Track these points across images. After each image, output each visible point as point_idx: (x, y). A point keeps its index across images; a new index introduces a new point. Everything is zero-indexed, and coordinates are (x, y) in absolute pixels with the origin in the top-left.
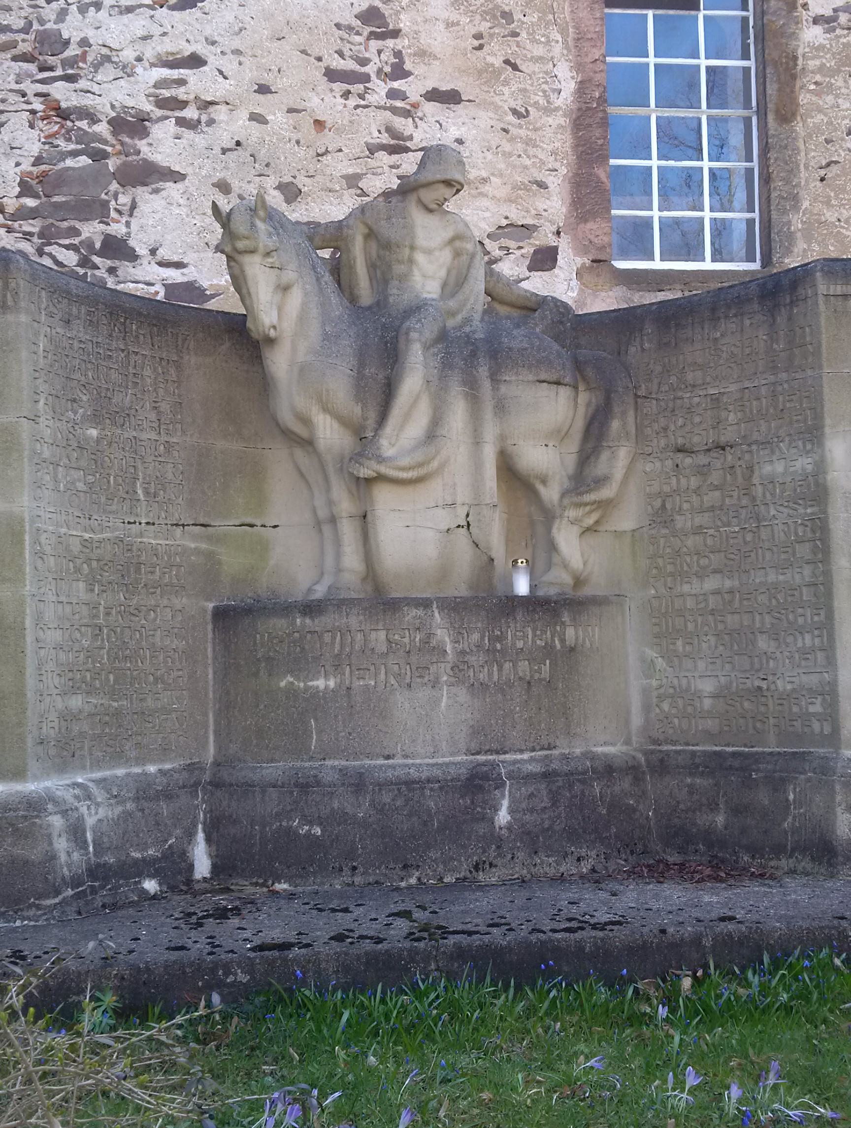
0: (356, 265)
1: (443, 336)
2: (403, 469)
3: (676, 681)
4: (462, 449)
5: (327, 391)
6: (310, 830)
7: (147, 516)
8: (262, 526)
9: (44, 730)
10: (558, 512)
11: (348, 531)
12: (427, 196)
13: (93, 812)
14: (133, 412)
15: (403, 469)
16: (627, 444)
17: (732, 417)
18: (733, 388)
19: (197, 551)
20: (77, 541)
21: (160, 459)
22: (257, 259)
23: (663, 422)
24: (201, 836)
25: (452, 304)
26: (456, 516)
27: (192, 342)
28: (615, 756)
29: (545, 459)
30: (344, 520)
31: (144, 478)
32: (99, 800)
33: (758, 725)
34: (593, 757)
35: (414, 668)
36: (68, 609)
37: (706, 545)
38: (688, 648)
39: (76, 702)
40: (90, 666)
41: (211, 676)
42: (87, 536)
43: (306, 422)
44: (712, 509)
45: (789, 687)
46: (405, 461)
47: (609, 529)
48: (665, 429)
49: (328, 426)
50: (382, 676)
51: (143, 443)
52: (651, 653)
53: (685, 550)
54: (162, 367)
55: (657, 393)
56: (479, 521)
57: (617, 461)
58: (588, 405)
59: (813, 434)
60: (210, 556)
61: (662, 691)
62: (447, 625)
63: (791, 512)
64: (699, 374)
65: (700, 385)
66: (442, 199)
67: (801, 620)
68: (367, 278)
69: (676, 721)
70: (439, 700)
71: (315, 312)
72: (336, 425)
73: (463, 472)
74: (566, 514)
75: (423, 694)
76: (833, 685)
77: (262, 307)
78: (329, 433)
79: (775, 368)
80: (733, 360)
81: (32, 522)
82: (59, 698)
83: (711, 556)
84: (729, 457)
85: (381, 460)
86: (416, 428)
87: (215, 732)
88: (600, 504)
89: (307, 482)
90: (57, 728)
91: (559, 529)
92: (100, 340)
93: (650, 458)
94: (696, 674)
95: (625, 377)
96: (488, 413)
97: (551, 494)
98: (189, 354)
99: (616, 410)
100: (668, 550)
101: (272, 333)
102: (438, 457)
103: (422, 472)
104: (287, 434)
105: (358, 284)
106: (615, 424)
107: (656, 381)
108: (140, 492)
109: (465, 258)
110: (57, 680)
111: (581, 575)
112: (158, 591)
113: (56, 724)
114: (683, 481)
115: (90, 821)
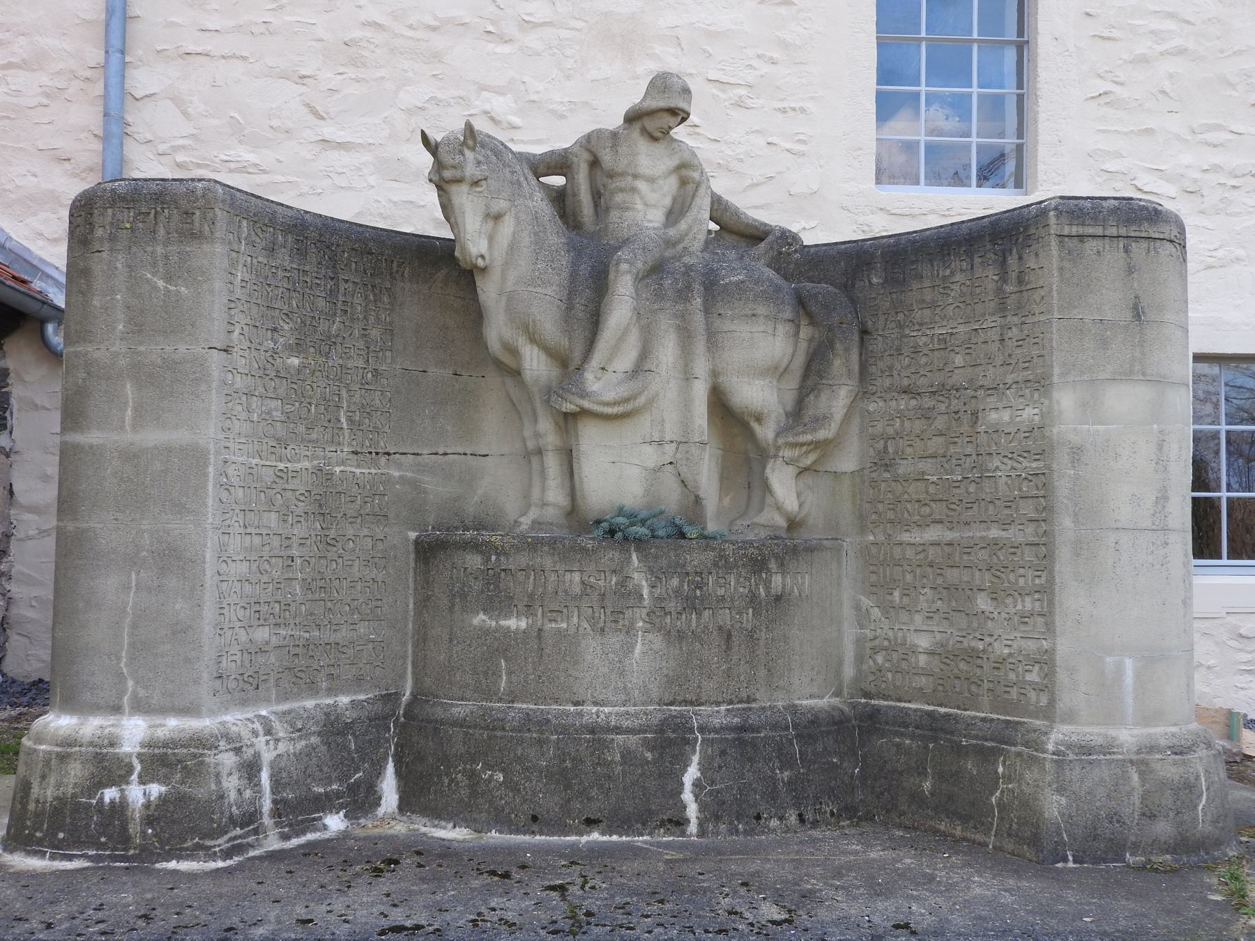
0: (577, 192)
2: (608, 404)
3: (891, 634)
4: (673, 383)
5: (534, 321)
6: (491, 776)
7: (350, 445)
9: (224, 664)
10: (772, 451)
11: (553, 464)
12: (651, 124)
13: (272, 747)
14: (340, 340)
15: (608, 404)
16: (850, 382)
17: (959, 360)
18: (961, 329)
20: (270, 471)
22: (464, 188)
24: (390, 768)
25: (672, 232)
26: (664, 453)
28: (821, 710)
29: (758, 394)
30: (550, 453)
32: (281, 734)
33: (973, 688)
34: (793, 709)
35: (608, 611)
36: (257, 540)
37: (927, 492)
38: (905, 600)
39: (262, 634)
40: (279, 598)
41: (411, 606)
42: (281, 466)
43: (514, 352)
45: (1006, 651)
46: (610, 396)
48: (891, 368)
49: (535, 356)
50: (575, 620)
52: (866, 602)
53: (906, 496)
54: (375, 295)
57: (837, 400)
58: (811, 340)
59: (1041, 384)
60: (415, 485)
61: (877, 642)
62: (644, 569)
63: (1015, 464)
67: (1021, 581)
68: (592, 205)
69: (890, 675)
70: (633, 647)
72: (543, 357)
73: (677, 406)
75: (615, 640)
76: (1051, 652)
77: (468, 237)
78: (535, 364)
79: (1005, 309)
81: (218, 452)
82: (242, 632)
85: (584, 395)
86: (625, 361)
87: (413, 663)
88: (816, 445)
89: (518, 412)
90: (239, 663)
92: (307, 268)
93: (874, 398)
94: (912, 628)
96: (700, 346)
97: (766, 432)
101: (480, 263)
103: (629, 407)
104: (499, 364)
106: (837, 363)
107: (882, 318)
108: (343, 420)
109: (690, 187)
110: (241, 613)
112: (359, 520)
113: (238, 658)
115: (267, 757)
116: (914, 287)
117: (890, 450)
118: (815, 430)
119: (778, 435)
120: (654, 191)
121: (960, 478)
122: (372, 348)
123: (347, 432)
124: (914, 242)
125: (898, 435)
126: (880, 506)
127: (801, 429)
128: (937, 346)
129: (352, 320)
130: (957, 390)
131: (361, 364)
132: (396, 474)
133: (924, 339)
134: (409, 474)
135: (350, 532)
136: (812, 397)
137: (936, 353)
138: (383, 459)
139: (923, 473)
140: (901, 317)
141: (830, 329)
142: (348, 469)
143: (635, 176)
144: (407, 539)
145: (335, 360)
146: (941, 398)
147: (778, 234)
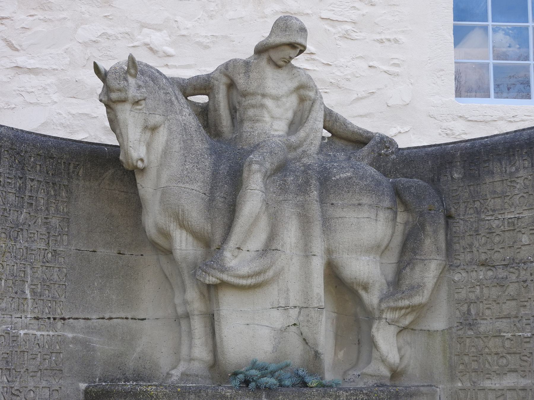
0: (217, 108)
1: (282, 168)
2: (243, 277)
4: (295, 260)
5: (183, 211)
7: (32, 312)
8: (132, 319)
11: (198, 326)
12: (275, 55)
14: (26, 227)
15: (243, 277)
17: (525, 239)
18: (526, 214)
19: (75, 340)
21: (47, 264)
22: (127, 106)
23: (468, 240)
26: (289, 317)
27: (82, 169)
29: (365, 268)
30: (196, 317)
31: (32, 281)
37: (504, 347)
43: (167, 235)
44: (508, 317)
47: (424, 328)
48: (471, 245)
51: (33, 252)
53: (487, 350)
55: (464, 215)
56: (308, 321)
57: (429, 272)
58: (406, 224)
60: (86, 344)
64: (498, 201)
65: (499, 210)
66: (288, 57)
71: (177, 146)
72: (190, 239)
73: (300, 279)
74: (384, 316)
77: (131, 144)
78: (184, 245)
80: (526, 190)
83: (508, 356)
84: (523, 273)
85: (223, 269)
86: (257, 242)
88: (412, 308)
89: (170, 284)
91: (378, 329)
93: (458, 270)
95: (437, 201)
96: (317, 229)
97: (372, 299)
98: (78, 179)
99: (429, 228)
100: (473, 349)
101: (140, 165)
102: (274, 268)
103: (260, 279)
104: (155, 245)
105: (221, 123)
106: (428, 242)
107: (463, 206)
108: (27, 292)
111: (397, 368)
112: (39, 374)
114: (485, 291)
116: (487, 181)
117: (473, 312)
118: (411, 296)
119: (381, 300)
120: (278, 106)
121: (529, 335)
122: (52, 233)
123: (30, 302)
124: (485, 145)
125: (479, 300)
126: (466, 358)
127: (399, 295)
128: (507, 228)
129: (37, 211)
130: (525, 263)
131: (42, 246)
132: (70, 335)
133: (497, 222)
134: (81, 336)
135: (31, 384)
136: (408, 269)
137: (507, 234)
138: (59, 324)
139: (500, 331)
140: (477, 204)
141: (421, 214)
142: (31, 332)
143: (264, 96)
144: (78, 389)
145: (22, 243)
146: (512, 270)
147: (378, 139)
